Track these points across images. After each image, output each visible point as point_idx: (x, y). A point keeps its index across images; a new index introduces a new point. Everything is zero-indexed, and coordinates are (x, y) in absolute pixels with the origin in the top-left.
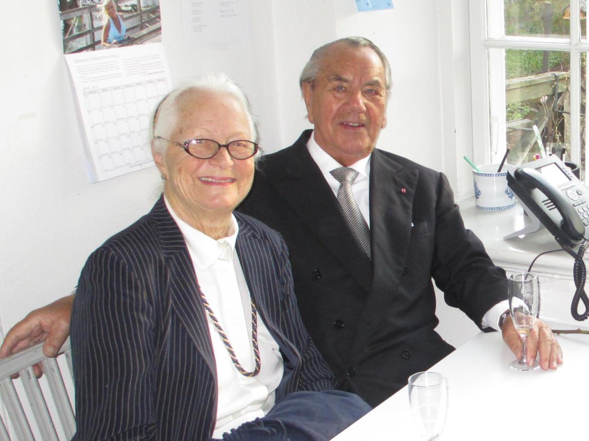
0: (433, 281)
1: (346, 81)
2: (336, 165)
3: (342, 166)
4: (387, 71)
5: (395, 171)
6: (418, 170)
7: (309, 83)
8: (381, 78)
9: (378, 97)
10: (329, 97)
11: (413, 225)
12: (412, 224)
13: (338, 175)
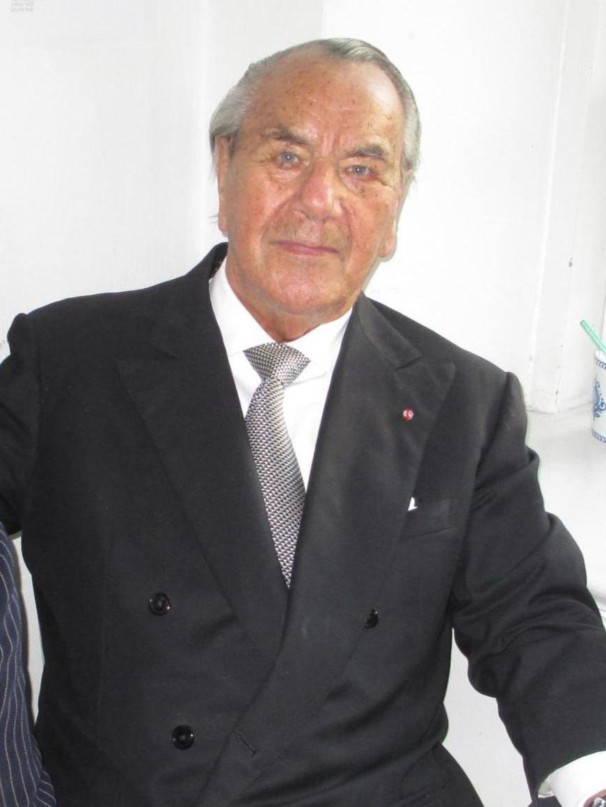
0: (453, 630)
1: (302, 143)
2: (261, 337)
3: (274, 342)
4: (411, 125)
5: (397, 363)
6: (453, 366)
7: (228, 139)
8: (391, 142)
9: (376, 185)
10: (260, 174)
11: (412, 506)
12: (413, 501)
13: (261, 360)
